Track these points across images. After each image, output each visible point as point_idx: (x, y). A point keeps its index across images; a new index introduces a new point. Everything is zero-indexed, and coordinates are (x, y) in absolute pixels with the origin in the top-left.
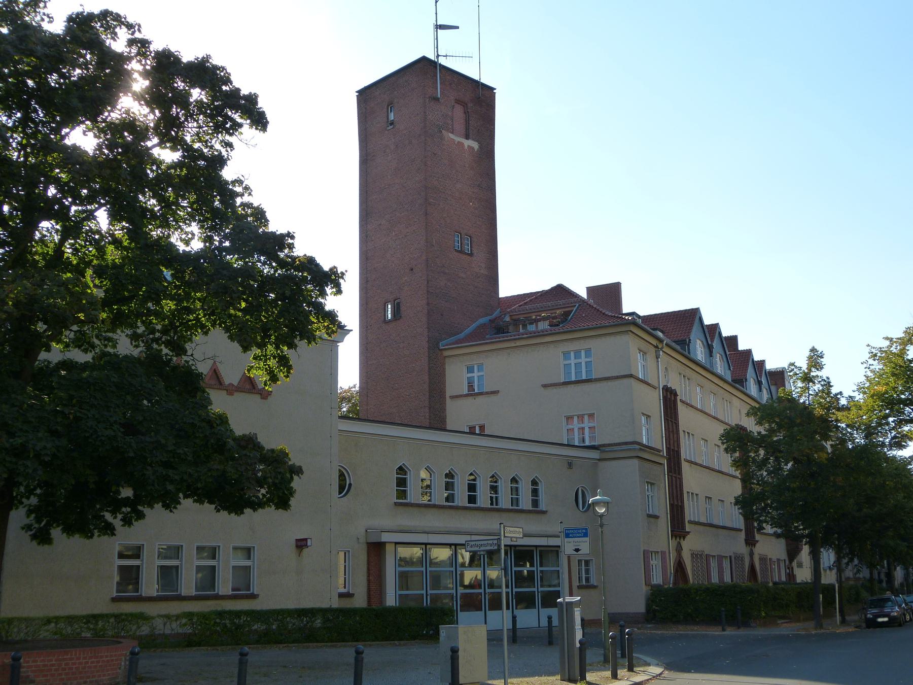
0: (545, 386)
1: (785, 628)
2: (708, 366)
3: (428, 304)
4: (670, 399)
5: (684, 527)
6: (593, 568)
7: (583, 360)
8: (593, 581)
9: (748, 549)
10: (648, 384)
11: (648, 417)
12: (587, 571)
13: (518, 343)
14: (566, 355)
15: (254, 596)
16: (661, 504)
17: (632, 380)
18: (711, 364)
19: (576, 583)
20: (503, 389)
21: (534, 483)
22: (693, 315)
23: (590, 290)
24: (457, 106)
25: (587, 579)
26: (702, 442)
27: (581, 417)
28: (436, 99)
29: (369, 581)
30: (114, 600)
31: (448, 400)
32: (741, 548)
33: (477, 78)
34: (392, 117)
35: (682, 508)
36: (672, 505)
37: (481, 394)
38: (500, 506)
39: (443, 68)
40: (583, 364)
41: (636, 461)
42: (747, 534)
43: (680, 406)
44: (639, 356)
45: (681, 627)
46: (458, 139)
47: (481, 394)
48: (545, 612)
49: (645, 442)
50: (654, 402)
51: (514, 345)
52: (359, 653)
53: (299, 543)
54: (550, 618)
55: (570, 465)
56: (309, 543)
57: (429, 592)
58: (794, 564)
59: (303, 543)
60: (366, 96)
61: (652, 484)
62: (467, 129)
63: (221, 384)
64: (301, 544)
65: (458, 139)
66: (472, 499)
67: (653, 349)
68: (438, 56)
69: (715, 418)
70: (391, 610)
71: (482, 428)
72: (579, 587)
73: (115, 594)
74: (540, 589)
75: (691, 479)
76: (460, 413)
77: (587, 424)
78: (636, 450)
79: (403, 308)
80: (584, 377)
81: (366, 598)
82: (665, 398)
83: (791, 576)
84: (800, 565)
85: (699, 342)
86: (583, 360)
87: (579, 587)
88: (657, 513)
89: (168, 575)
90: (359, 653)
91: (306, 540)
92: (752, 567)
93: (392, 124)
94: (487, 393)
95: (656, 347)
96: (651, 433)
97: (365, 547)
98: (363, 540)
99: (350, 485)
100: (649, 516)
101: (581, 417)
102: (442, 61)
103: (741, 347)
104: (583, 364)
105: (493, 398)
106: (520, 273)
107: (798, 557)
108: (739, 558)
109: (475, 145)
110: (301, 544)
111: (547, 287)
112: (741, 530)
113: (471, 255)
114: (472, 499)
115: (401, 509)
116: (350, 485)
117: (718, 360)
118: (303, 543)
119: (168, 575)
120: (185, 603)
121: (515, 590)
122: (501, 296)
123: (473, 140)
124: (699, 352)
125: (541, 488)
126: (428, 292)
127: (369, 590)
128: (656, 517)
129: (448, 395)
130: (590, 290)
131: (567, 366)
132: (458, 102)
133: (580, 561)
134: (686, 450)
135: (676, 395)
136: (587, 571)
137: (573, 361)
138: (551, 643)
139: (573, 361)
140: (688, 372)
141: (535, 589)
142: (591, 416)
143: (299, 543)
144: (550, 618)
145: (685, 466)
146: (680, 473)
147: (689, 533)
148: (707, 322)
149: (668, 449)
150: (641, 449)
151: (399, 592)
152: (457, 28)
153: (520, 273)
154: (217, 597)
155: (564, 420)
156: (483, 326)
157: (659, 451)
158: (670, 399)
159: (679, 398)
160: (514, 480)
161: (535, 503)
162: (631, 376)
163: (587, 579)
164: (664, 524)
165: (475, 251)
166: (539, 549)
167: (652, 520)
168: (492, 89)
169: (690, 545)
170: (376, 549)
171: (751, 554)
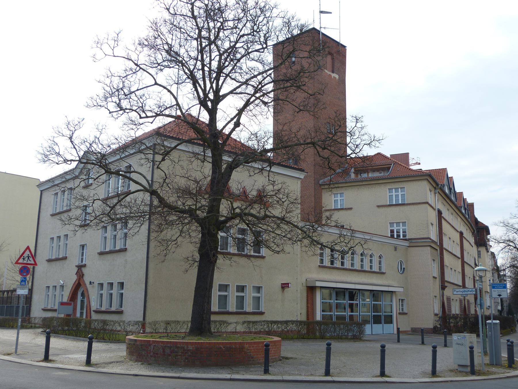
0: (378, 206)
3: (314, 160)
6: (405, 303)
7: (400, 193)
13: (364, 183)
14: (390, 190)
15: (262, 313)
17: (427, 205)
21: (380, 257)
23: (391, 155)
29: (308, 307)
33: (338, 41)
37: (342, 209)
39: (323, 34)
40: (400, 196)
41: (429, 248)
47: (342, 209)
50: (433, 216)
51: (361, 184)
52: (329, 345)
53: (284, 286)
55: (396, 249)
57: (361, 314)
65: (329, 73)
68: (321, 28)
70: (318, 322)
80: (400, 202)
81: (306, 315)
86: (400, 193)
89: (240, 300)
90: (329, 345)
91: (288, 284)
94: (346, 209)
96: (434, 236)
97: (305, 288)
98: (304, 285)
101: (398, 224)
102: (323, 31)
104: (400, 196)
105: (349, 212)
109: (337, 76)
110: (285, 286)
115: (321, 269)
119: (240, 300)
121: (373, 314)
130: (391, 155)
131: (391, 196)
133: (399, 299)
137: (394, 194)
138: (446, 346)
139: (394, 194)
141: (333, 313)
142: (404, 223)
143: (284, 286)
147: (446, 287)
148: (449, 176)
152: (331, 13)
154: (246, 313)
161: (380, 268)
166: (348, 290)
168: (345, 47)
170: (311, 290)
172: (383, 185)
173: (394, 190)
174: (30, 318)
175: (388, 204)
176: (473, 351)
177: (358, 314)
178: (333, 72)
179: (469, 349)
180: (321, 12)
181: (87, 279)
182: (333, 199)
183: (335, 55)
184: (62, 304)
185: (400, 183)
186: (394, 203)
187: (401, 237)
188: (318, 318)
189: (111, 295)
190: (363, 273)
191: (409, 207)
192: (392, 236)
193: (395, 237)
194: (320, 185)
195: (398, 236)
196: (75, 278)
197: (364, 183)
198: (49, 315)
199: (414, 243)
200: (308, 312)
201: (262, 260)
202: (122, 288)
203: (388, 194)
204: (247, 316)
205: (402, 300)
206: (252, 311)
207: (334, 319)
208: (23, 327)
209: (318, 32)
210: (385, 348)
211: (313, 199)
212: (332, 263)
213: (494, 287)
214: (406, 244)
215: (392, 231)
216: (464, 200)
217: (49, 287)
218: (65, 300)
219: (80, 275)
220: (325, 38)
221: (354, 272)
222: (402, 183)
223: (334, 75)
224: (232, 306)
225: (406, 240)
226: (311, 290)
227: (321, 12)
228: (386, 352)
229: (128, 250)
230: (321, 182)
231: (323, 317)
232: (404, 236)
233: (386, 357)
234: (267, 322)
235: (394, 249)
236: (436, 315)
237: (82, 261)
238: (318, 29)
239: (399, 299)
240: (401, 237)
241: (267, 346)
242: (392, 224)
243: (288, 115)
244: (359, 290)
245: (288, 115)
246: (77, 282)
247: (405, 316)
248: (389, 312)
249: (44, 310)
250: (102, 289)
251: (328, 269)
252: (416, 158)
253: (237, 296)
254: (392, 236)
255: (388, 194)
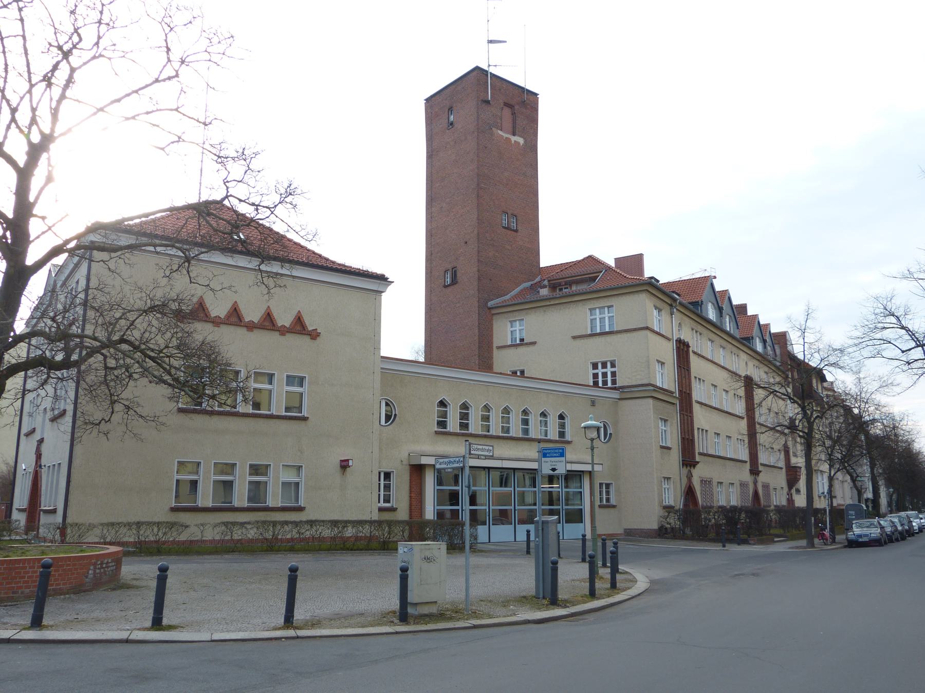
0: (574, 338)
1: (780, 547)
2: (719, 324)
3: (478, 271)
4: (682, 349)
5: (694, 457)
7: (606, 315)
8: (613, 501)
9: (753, 477)
10: (663, 336)
11: (663, 364)
12: (608, 493)
13: (552, 303)
15: (300, 509)
16: (672, 438)
18: (721, 322)
19: (598, 503)
20: (548, 345)
21: (561, 417)
22: (706, 282)
24: (505, 108)
25: (608, 500)
26: (724, 393)
27: (604, 365)
28: (488, 102)
30: (174, 510)
31: (495, 351)
32: (746, 476)
33: (523, 85)
34: (452, 118)
35: (693, 441)
36: (683, 439)
38: (530, 436)
39: (493, 75)
40: (607, 319)
41: (651, 401)
42: (751, 466)
43: (692, 357)
44: (655, 312)
45: (695, 543)
46: (505, 135)
48: (522, 529)
49: (659, 384)
50: (668, 352)
54: (528, 532)
55: (593, 403)
56: (350, 463)
57: (517, 507)
58: (793, 491)
59: (345, 463)
60: (428, 100)
61: (665, 421)
62: (514, 128)
63: (274, 325)
64: (344, 465)
65: (505, 135)
66: (464, 426)
67: (668, 308)
69: (723, 367)
70: (429, 522)
71: (522, 372)
72: (600, 506)
73: (173, 505)
74: (565, 507)
75: (700, 418)
76: (504, 360)
77: (609, 370)
78: (651, 391)
79: (458, 275)
80: (607, 330)
81: (408, 511)
82: (678, 348)
83: (790, 501)
84: (798, 491)
85: (710, 304)
86: (606, 315)
87: (600, 506)
88: (669, 445)
89: (257, 490)
91: (348, 460)
92: (756, 493)
93: (452, 124)
95: (671, 305)
96: (666, 378)
97: (408, 468)
98: (405, 462)
99: (395, 415)
100: (662, 447)
102: (493, 70)
103: (750, 313)
104: (607, 319)
106: (556, 248)
107: (797, 486)
108: (743, 485)
109: (521, 141)
110: (344, 465)
111: (580, 258)
112: (746, 462)
113: (516, 231)
114: (464, 426)
115: (440, 437)
116: (395, 415)
117: (727, 320)
118: (345, 463)
119: (257, 490)
120: (238, 514)
122: (542, 265)
123: (519, 136)
124: (712, 314)
125: (567, 421)
126: (479, 260)
127: (411, 505)
128: (669, 448)
129: (495, 345)
130: (617, 260)
132: (507, 105)
133: (601, 484)
134: (698, 393)
135: (688, 346)
136: (608, 493)
140: (700, 328)
144: (528, 532)
145: (696, 408)
146: (691, 412)
149: (680, 391)
150: (654, 390)
151: (437, 508)
153: (556, 248)
155: (590, 367)
156: (525, 289)
157: (672, 393)
158: (682, 349)
159: (691, 349)
160: (543, 414)
161: (562, 434)
162: (647, 328)
163: (608, 500)
164: (675, 456)
165: (519, 228)
167: (665, 450)
168: (536, 95)
169: (698, 473)
170: (418, 470)
171: (755, 483)
172: (581, 304)
173: (597, 310)
174: (10, 522)
175: (589, 332)
176: (407, 575)
177: (512, 507)
178: (514, 135)
179: (400, 572)
180: (490, 42)
182: (509, 329)
183: (517, 107)
185: (606, 300)
186: (598, 331)
187: (609, 385)
188: (430, 513)
190: (527, 443)
191: (619, 336)
192: (596, 384)
193: (600, 385)
194: (490, 309)
195: (605, 383)
197: (552, 303)
199: (627, 393)
201: (303, 422)
203: (589, 318)
204: (269, 513)
205: (608, 486)
206: (280, 505)
209: (485, 72)
210: (168, 573)
211: (477, 331)
213: (545, 455)
214: (615, 395)
215: (595, 376)
216: (764, 329)
220: (494, 79)
221: (509, 441)
222: (610, 299)
223: (514, 139)
225: (615, 389)
226: (418, 470)
227: (490, 42)
228: (168, 581)
229: (309, 422)
230: (490, 304)
231: (440, 515)
232: (614, 382)
233: (299, 585)
234: (312, 523)
235: (590, 402)
236: (669, 509)
238: (486, 68)
239: (601, 484)
240: (609, 385)
241: (46, 566)
242: (595, 366)
244: (514, 469)
247: (612, 510)
248: (530, 505)
251: (455, 437)
252: (709, 270)
253: (250, 482)
254: (596, 384)
255: (589, 318)
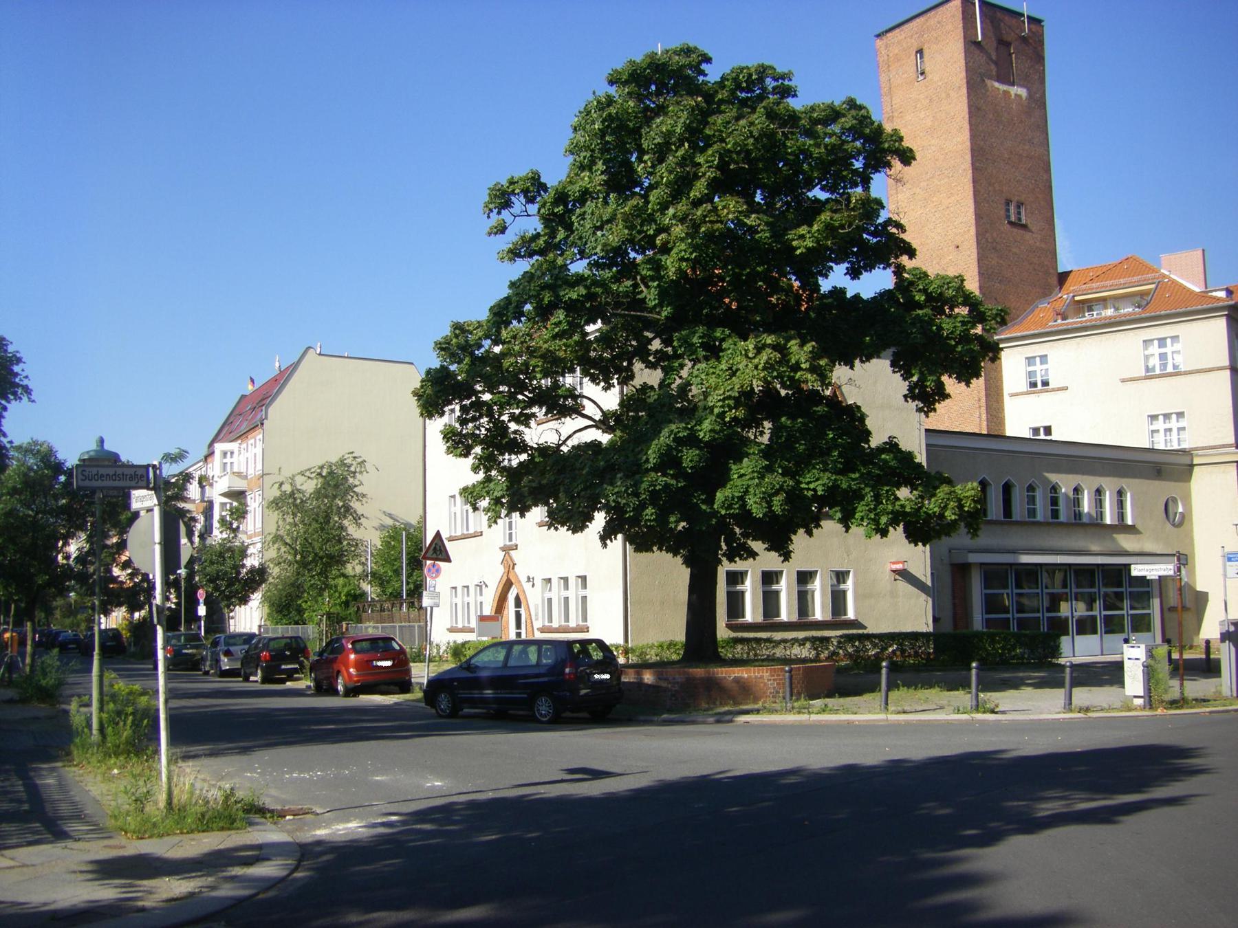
0: (1123, 381)
29: (954, 605)
89: (803, 601)
109: (1022, 92)
119: (803, 601)
142: (1180, 415)
181: (521, 572)
184: (482, 618)
185: (1168, 327)
189: (566, 599)
196: (500, 571)
198: (460, 638)
200: (955, 615)
202: (584, 586)
207: (1014, 628)
208: (892, 686)
212: (1007, 511)
217: (455, 588)
218: (488, 610)
219: (510, 565)
224: (786, 612)
231: (988, 623)
237: (510, 539)
243: (918, 191)
245: (918, 191)
246: (505, 578)
249: (452, 630)
250: (566, 587)
